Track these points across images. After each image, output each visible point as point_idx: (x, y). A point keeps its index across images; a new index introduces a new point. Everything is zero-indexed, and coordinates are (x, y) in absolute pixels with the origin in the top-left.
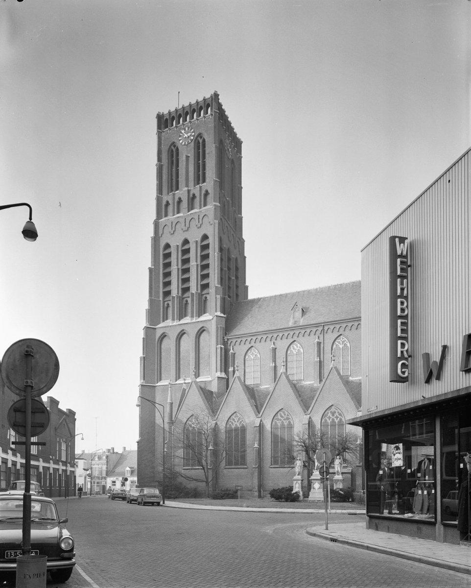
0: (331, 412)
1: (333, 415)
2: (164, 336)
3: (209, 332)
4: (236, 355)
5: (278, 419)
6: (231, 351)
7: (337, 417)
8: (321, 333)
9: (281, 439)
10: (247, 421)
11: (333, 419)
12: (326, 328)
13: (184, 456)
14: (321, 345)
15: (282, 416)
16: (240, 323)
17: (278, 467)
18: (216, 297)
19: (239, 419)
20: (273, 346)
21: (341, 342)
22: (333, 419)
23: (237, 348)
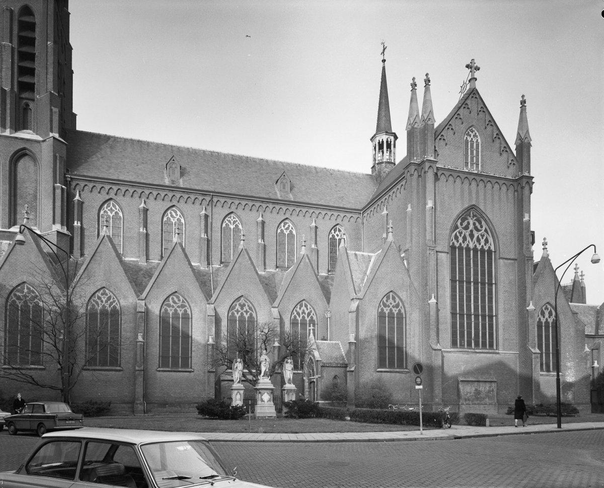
0: (240, 305)
1: (242, 309)
3: (34, 159)
4: (84, 206)
5: (169, 306)
6: (77, 197)
7: (247, 312)
8: (208, 205)
9: (91, 344)
10: (123, 303)
11: (242, 314)
12: (215, 199)
13: (43, 343)
14: (209, 219)
15: (174, 302)
16: (86, 161)
17: (169, 371)
18: (51, 110)
19: (109, 298)
20: (143, 205)
21: (232, 222)
22: (242, 314)
23: (86, 195)
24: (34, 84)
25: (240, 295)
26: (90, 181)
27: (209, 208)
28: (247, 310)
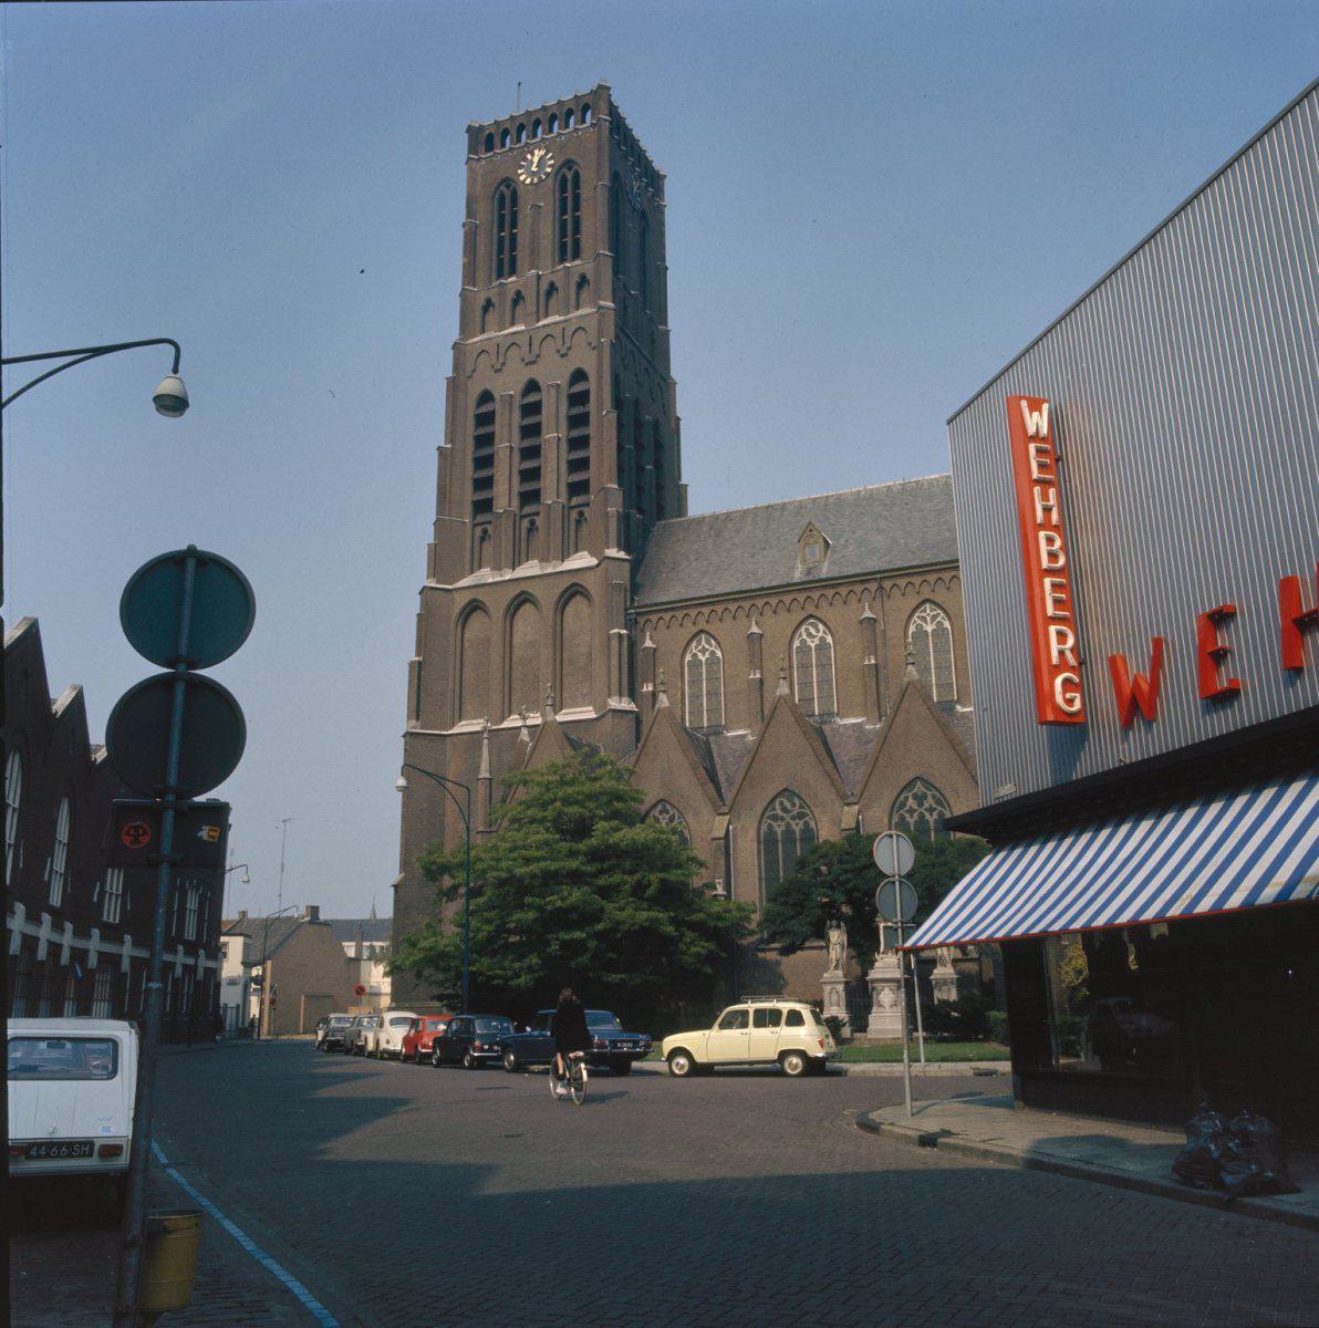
0: (915, 797)
1: (920, 805)
2: (474, 607)
5: (775, 818)
7: (931, 810)
15: (785, 810)
21: (929, 619)
24: (540, 489)
25: (911, 776)
26: (666, 610)
27: (878, 604)
28: (931, 806)
